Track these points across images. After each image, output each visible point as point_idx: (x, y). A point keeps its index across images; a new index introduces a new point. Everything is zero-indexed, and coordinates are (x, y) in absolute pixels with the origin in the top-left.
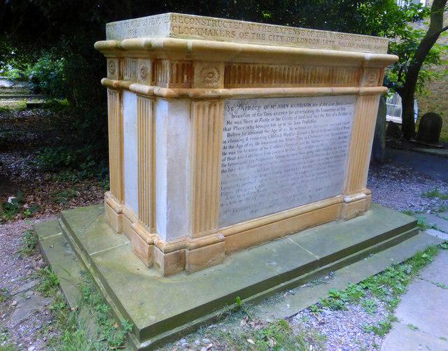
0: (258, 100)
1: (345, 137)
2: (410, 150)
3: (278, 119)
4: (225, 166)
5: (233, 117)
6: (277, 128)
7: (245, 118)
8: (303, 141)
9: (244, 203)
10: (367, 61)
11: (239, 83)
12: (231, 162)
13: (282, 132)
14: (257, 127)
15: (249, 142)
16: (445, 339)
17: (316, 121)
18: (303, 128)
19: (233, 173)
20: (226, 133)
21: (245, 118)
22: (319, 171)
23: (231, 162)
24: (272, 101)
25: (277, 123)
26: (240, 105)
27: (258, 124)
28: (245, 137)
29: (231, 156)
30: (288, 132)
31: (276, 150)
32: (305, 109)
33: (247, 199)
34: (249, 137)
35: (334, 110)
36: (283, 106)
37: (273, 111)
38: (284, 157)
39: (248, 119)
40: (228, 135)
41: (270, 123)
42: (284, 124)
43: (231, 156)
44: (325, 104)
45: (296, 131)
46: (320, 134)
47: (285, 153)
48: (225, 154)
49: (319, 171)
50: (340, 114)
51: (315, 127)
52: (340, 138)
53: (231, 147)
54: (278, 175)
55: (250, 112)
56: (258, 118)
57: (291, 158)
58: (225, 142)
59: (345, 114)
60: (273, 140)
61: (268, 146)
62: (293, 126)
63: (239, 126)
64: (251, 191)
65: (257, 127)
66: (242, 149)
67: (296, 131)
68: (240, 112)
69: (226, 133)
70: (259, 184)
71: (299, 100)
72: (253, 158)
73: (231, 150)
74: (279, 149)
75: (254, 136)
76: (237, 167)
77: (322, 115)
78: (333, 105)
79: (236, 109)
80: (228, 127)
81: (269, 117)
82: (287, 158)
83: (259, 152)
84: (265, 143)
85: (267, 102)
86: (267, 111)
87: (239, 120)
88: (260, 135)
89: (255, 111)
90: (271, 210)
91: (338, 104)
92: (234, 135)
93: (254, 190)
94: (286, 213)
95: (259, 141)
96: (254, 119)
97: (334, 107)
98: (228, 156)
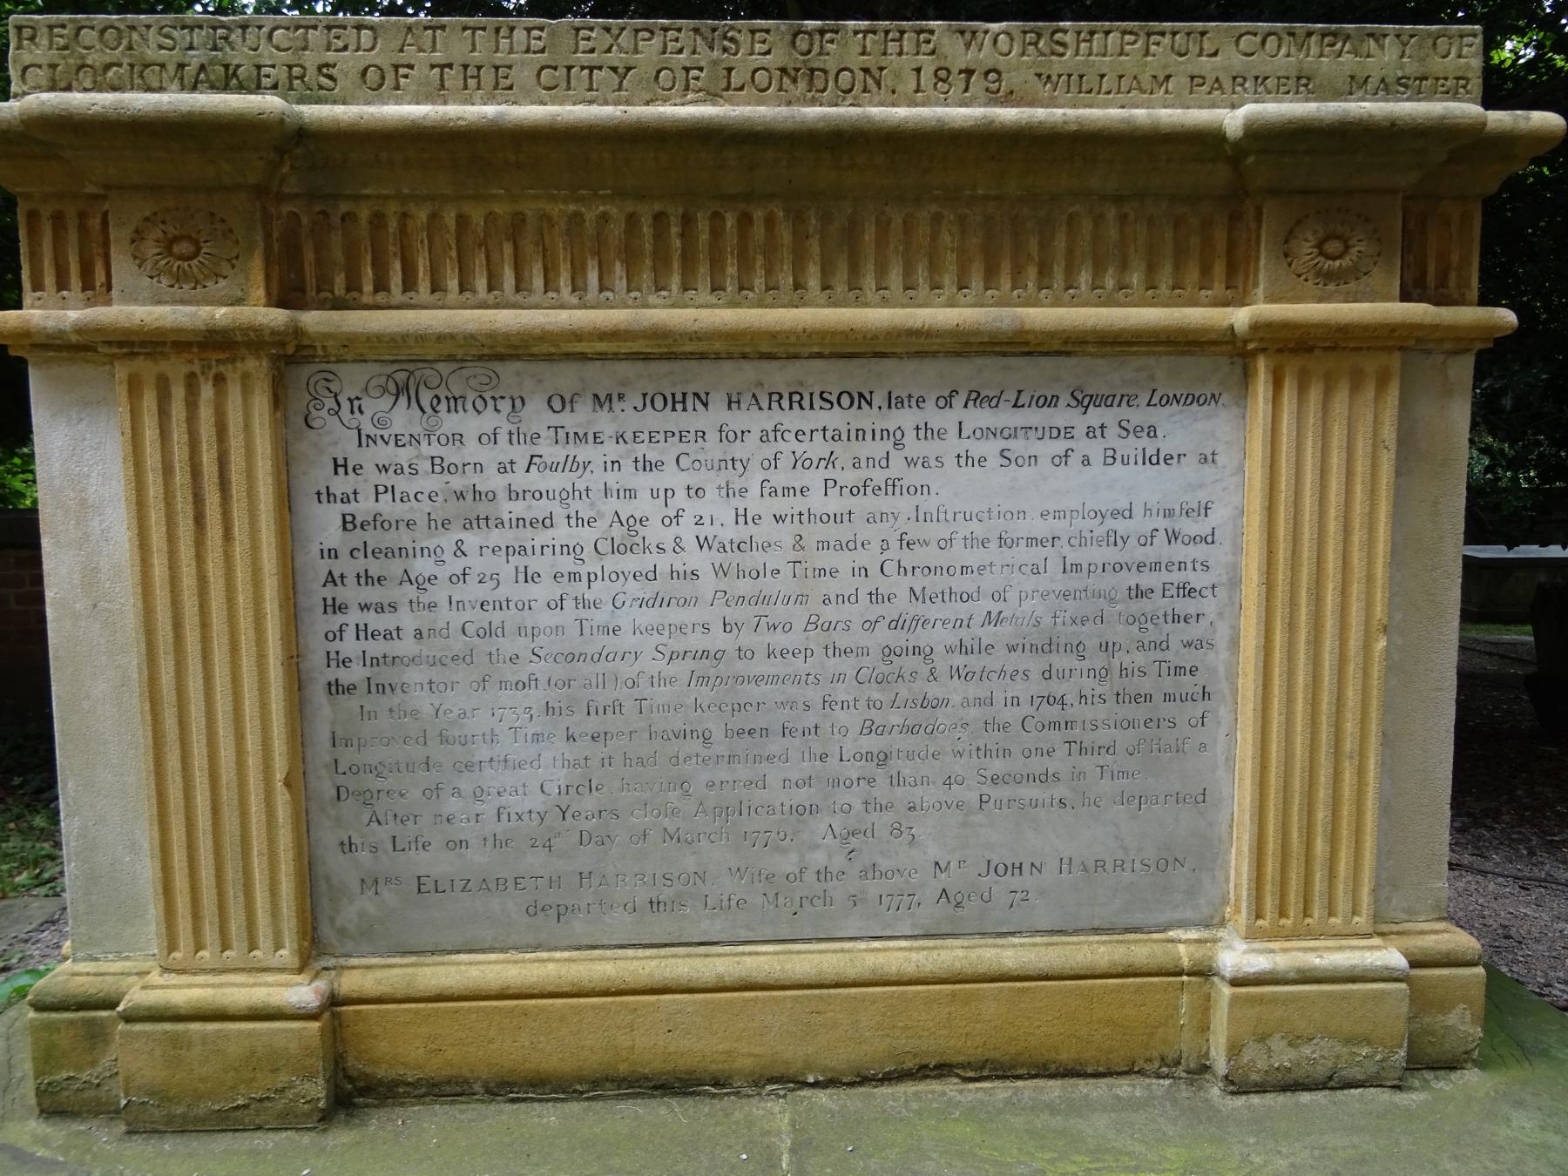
0: (508, 370)
1: (1187, 591)
2: (283, 344)
3: (647, 466)
4: (345, 663)
5: (364, 440)
6: (643, 505)
7: (435, 450)
8: (844, 584)
9: (479, 858)
10: (1241, 139)
11: (935, 286)
12: (376, 648)
13: (687, 531)
14: (513, 495)
15: (476, 563)
16: (328, 488)
17: (924, 489)
18: (836, 518)
19: (395, 699)
20: (333, 513)
21: (435, 450)
22: (997, 766)
23: (376, 648)
24: (601, 377)
25: (644, 481)
26: (401, 390)
27: (519, 480)
28: (447, 540)
29: (375, 621)
30: (730, 533)
31: (649, 616)
32: (835, 418)
33: (499, 843)
34: (472, 539)
35: (1066, 432)
36: (676, 402)
37: (605, 423)
38: (718, 656)
39: (451, 455)
40: (348, 523)
41: (595, 479)
42: (696, 492)
43: (375, 621)
44: (976, 398)
45: (786, 533)
46: (973, 557)
47: (717, 640)
48: (337, 608)
49: (997, 766)
50: (1111, 458)
51: (919, 516)
52: (1139, 593)
53: (365, 578)
54: (695, 746)
55: (469, 423)
56: (520, 454)
57: (762, 666)
58: (333, 554)
59: (1154, 460)
60: (629, 563)
61: (600, 590)
62: (754, 503)
63: (403, 484)
64: (516, 803)
65: (513, 495)
66: (439, 593)
67: (786, 533)
68: (403, 419)
69: (333, 513)
70: (561, 776)
71: (780, 376)
72: (508, 646)
73: (371, 594)
74: (675, 615)
75: (496, 537)
76: (414, 675)
77: (963, 459)
78: (1051, 402)
79: (376, 405)
80: (341, 485)
81: (584, 452)
82: (741, 667)
83: (547, 619)
84: (574, 576)
85: (565, 377)
86: (568, 420)
87: (404, 455)
88: (543, 537)
89: (488, 421)
90: (662, 926)
91: (1083, 401)
92: (377, 522)
93: (536, 802)
94: (762, 962)
95: (535, 563)
96: (488, 456)
97: (1062, 416)
98: (354, 617)
